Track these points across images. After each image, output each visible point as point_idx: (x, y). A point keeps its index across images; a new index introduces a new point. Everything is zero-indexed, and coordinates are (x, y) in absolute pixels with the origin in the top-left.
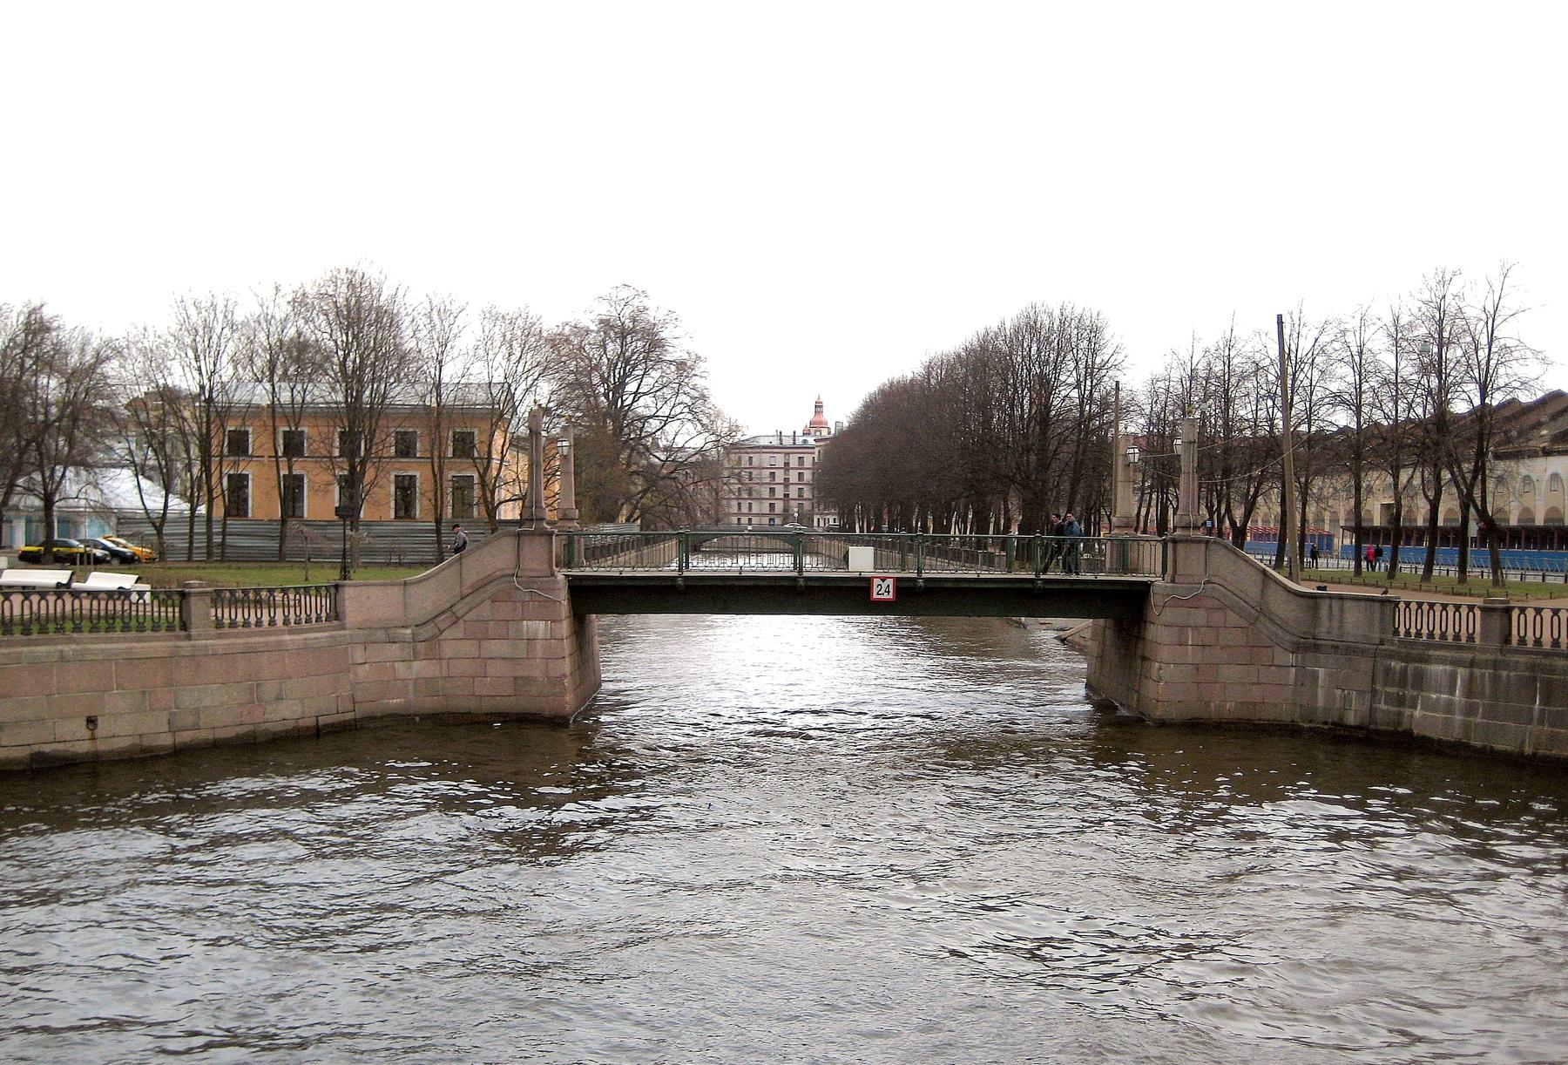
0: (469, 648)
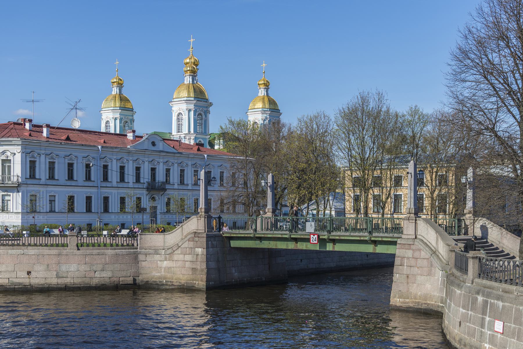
0: (181, 257)
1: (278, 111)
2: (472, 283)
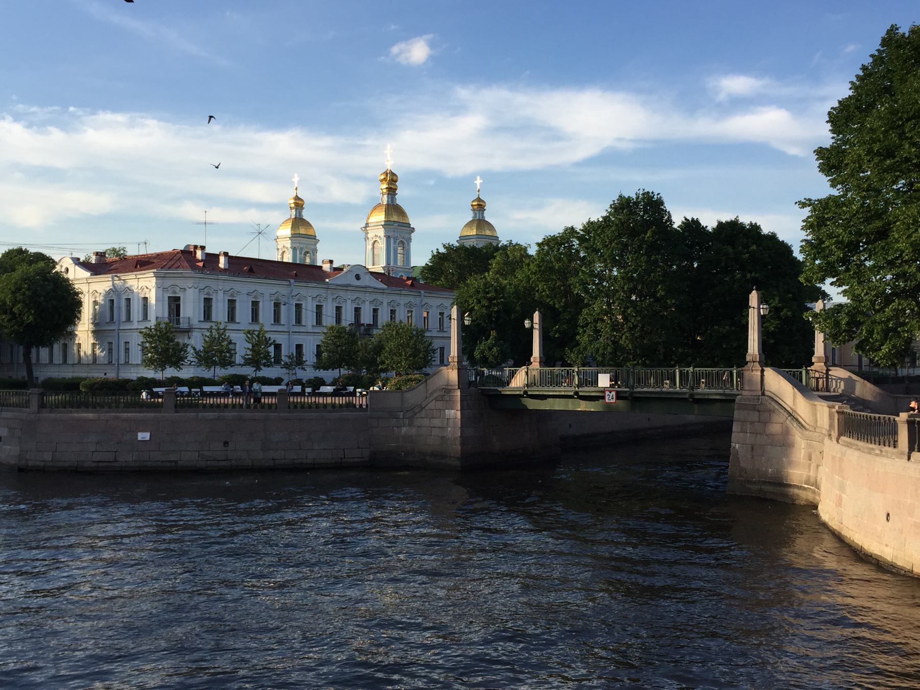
1: (496, 238)
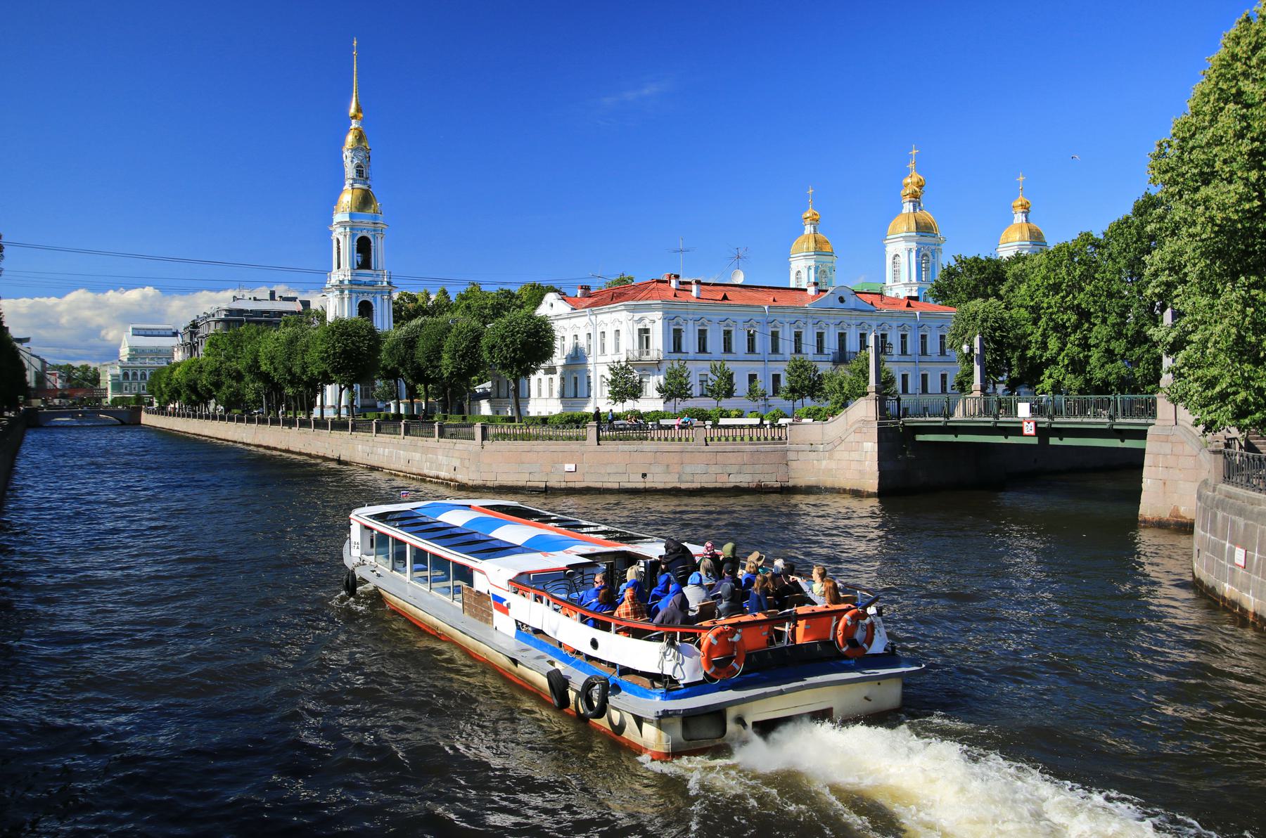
0: (846, 455)
2: (1214, 491)
